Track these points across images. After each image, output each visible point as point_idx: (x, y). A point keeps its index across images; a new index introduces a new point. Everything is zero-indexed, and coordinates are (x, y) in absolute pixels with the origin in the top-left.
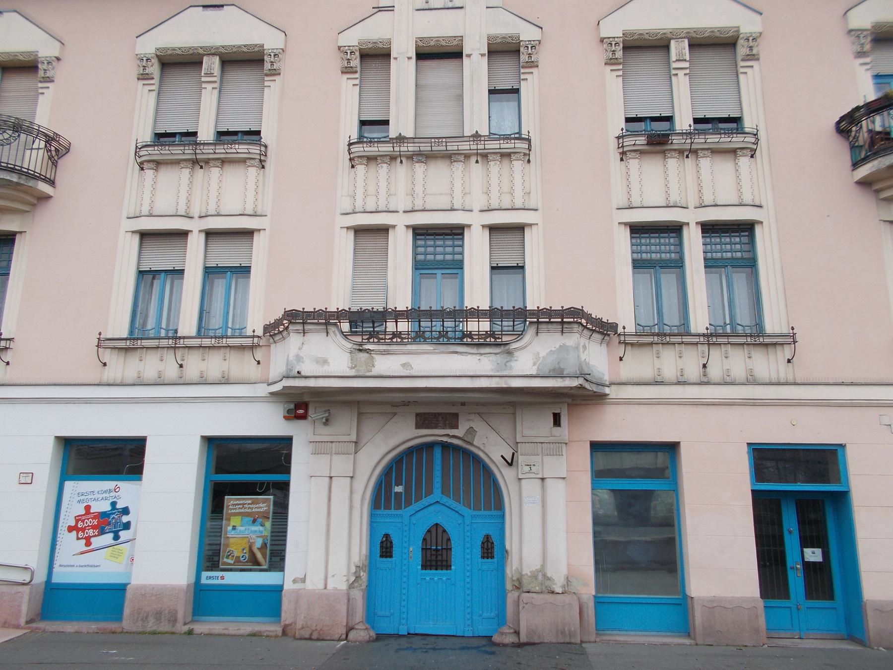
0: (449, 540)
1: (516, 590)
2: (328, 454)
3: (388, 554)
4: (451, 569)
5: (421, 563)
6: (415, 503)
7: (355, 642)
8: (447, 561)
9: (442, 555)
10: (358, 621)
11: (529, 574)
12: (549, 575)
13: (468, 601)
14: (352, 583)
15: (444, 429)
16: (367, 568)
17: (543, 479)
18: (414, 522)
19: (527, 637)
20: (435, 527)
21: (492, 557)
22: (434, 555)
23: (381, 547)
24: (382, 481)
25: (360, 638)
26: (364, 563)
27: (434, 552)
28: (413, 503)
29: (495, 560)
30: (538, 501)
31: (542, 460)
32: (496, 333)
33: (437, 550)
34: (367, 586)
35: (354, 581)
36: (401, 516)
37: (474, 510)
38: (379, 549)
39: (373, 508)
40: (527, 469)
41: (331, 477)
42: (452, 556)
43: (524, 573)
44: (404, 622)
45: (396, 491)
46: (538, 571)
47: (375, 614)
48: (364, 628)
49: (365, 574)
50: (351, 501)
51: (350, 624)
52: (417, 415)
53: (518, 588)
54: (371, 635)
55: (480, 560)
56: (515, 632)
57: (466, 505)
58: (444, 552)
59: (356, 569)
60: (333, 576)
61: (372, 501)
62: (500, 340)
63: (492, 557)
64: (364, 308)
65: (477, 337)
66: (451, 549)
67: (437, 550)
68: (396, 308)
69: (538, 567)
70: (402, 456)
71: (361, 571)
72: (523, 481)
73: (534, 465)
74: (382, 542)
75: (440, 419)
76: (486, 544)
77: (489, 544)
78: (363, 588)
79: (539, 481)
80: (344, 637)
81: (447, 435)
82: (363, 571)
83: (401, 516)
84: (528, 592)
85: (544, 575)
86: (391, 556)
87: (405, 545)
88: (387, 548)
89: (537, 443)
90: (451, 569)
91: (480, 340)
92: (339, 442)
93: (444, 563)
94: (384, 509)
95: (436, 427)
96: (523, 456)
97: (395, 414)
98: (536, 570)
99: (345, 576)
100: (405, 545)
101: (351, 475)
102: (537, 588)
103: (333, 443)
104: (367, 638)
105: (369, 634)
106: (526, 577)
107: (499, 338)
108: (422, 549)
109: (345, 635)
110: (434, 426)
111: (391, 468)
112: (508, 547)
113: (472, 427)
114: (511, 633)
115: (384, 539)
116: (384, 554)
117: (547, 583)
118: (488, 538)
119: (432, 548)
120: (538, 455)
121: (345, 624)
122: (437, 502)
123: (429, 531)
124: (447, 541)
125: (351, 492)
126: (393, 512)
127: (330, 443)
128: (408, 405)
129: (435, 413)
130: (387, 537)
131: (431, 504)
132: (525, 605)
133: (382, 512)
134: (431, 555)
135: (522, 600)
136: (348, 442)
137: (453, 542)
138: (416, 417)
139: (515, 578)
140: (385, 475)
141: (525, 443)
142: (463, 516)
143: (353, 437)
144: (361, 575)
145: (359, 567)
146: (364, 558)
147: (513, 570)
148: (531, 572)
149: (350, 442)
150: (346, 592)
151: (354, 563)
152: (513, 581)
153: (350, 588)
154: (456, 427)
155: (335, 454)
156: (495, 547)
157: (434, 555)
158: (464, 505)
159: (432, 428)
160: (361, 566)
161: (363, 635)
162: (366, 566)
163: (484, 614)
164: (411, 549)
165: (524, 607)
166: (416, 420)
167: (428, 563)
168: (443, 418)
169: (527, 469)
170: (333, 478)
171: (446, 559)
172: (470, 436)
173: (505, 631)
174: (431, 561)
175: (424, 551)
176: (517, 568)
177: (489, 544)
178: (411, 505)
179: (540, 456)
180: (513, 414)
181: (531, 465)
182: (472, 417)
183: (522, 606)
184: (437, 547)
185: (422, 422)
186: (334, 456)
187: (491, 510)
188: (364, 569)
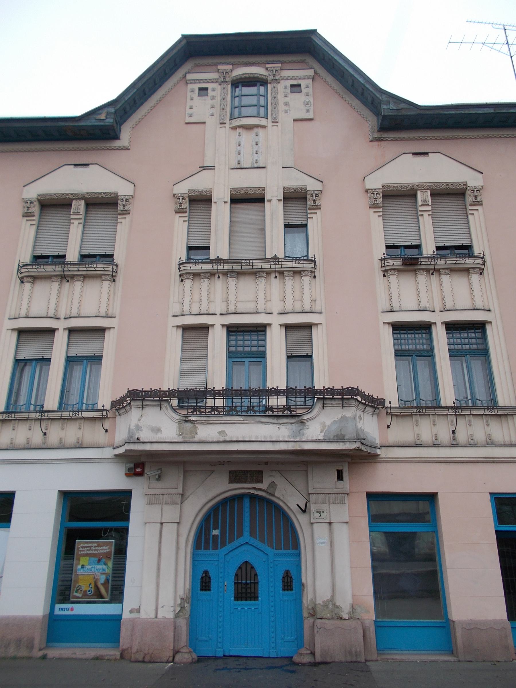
0: (256, 575)
5: (233, 595)
7: (180, 663)
8: (255, 593)
11: (322, 604)
12: (338, 604)
14: (178, 613)
15: (251, 483)
18: (228, 560)
23: (202, 582)
24: (202, 526)
25: (185, 660)
31: (329, 507)
32: (291, 407)
34: (190, 615)
36: (218, 555)
38: (199, 583)
39: (195, 548)
40: (317, 515)
41: (162, 524)
42: (259, 589)
43: (317, 602)
45: (213, 534)
46: (328, 601)
47: (197, 639)
48: (187, 651)
49: (188, 605)
51: (176, 649)
52: (231, 472)
58: (253, 585)
59: (181, 601)
60: (163, 607)
62: (295, 413)
63: (291, 590)
64: (189, 388)
65: (277, 410)
66: (258, 583)
67: (246, 584)
68: (333, 387)
69: (329, 597)
71: (185, 602)
72: (315, 525)
73: (323, 512)
74: (202, 578)
75: (249, 475)
76: (286, 578)
77: (289, 578)
79: (327, 525)
80: (171, 659)
82: (187, 603)
83: (218, 555)
84: (321, 619)
85: (334, 604)
91: (279, 413)
92: (169, 494)
93: (253, 595)
95: (245, 482)
97: (213, 472)
98: (328, 600)
104: (190, 660)
105: (192, 657)
106: (319, 606)
107: (294, 411)
112: (304, 581)
115: (204, 575)
116: (204, 588)
117: (337, 610)
118: (287, 573)
122: (247, 543)
123: (240, 568)
125: (178, 535)
126: (211, 552)
130: (206, 574)
131: (242, 545)
132: (318, 630)
133: (202, 552)
134: (242, 588)
139: (310, 607)
141: (316, 494)
142: (267, 554)
143: (180, 491)
144: (185, 606)
145: (184, 599)
146: (188, 592)
148: (323, 602)
149: (178, 494)
150: (173, 620)
151: (180, 596)
152: (309, 609)
153: (176, 617)
154: (261, 481)
155: (165, 504)
160: (185, 598)
161: (187, 657)
164: (226, 584)
165: (318, 631)
166: (230, 476)
167: (240, 595)
168: (250, 475)
174: (242, 593)
175: (236, 585)
176: (312, 599)
177: (289, 578)
178: (226, 545)
179: (328, 504)
184: (246, 581)
186: (166, 507)
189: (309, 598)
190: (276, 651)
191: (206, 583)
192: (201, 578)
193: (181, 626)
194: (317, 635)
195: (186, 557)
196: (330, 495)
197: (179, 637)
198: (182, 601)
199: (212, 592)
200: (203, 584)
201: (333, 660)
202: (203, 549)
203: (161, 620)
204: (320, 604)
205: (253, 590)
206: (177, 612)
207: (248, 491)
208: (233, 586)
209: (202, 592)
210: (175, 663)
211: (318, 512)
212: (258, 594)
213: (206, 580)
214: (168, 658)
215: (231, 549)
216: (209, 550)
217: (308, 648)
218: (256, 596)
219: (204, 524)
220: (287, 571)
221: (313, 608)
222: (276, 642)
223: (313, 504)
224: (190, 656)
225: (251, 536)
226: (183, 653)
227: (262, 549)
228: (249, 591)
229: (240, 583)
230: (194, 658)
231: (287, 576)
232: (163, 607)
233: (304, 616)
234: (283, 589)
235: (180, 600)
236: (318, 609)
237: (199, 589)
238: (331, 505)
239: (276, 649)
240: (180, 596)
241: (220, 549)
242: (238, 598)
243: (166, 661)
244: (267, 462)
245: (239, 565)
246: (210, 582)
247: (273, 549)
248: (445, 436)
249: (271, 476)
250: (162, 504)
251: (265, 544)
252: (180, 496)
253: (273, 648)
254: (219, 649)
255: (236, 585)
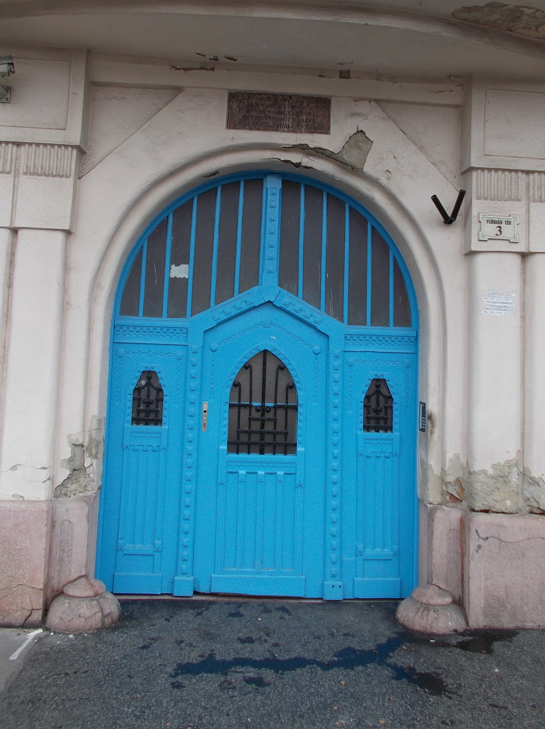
0: (291, 387)
1: (451, 504)
2: (9, 173)
3: (152, 416)
4: (294, 452)
5: (226, 437)
6: (216, 304)
7: (66, 632)
8: (286, 434)
9: (275, 421)
10: (74, 575)
11: (491, 472)
12: (536, 474)
13: (334, 523)
14: (63, 485)
15: (294, 132)
16: (102, 448)
17: (524, 256)
18: (214, 346)
19: (486, 615)
20: (260, 361)
21: (388, 428)
22: (256, 419)
23: (137, 400)
24: (141, 252)
25: (79, 623)
26: (94, 436)
27: (256, 415)
28: (212, 304)
29: (395, 434)
30: (513, 305)
31: (528, 211)
33: (263, 409)
34: (100, 488)
35: (68, 478)
36: (185, 331)
37: (349, 323)
38: (130, 404)
39: (118, 309)
40: (491, 230)
41: (15, 231)
42: (300, 424)
43: (477, 467)
44: (184, 566)
45: (172, 276)
46: (509, 464)
47: (118, 549)
48: (90, 593)
49: (95, 462)
50: (65, 289)
51: (55, 583)
52: (233, 96)
53: (455, 500)
54: (107, 611)
55: (362, 433)
56: (454, 602)
57: (331, 310)
58: (281, 414)
59: (73, 451)
60: (14, 468)
61: (116, 298)
63: (388, 428)
66: (295, 408)
67: (263, 409)
69: (512, 456)
70: (189, 198)
71: (87, 454)
72: (480, 260)
73: (508, 223)
74: (138, 390)
75: (287, 109)
76: (373, 399)
77: (382, 399)
78: (89, 493)
79: (517, 259)
80: (37, 616)
81: (303, 148)
82: (91, 455)
83: (185, 331)
84: (486, 511)
85: (524, 474)
86: (158, 422)
87: (192, 397)
88: (148, 403)
89: (516, 171)
90: (294, 452)
92: (38, 145)
93: (280, 439)
94: (146, 314)
95: (276, 127)
96: (482, 201)
97: (178, 90)
98: (508, 461)
99: (45, 468)
100: (192, 397)
101: (67, 227)
102: (508, 503)
103: (23, 148)
104: (96, 621)
105: (102, 610)
106: (482, 478)
108: (231, 406)
109: (41, 612)
110: (271, 124)
111: (165, 223)
112: (433, 407)
113: (362, 131)
114: (443, 606)
115: (143, 382)
116: (142, 415)
117: (530, 491)
118: (378, 386)
119: (254, 404)
120: (518, 200)
121: (41, 586)
122: (269, 302)
123: (247, 367)
124: (287, 390)
125: (66, 267)
126: (164, 321)
127: (15, 148)
128: (213, 69)
129: (275, 96)
130: (149, 379)
131: (255, 308)
132: (481, 542)
133: (140, 320)
134: (250, 420)
135: (477, 531)
136: (60, 146)
137: (300, 393)
138: (229, 101)
139: (450, 478)
140: (149, 238)
141: (490, 170)
142: (328, 336)
143: (75, 138)
144: (86, 465)
145: (82, 446)
146: (95, 426)
147: (447, 460)
148: (494, 466)
149: (66, 146)
150: (44, 507)
151: (69, 436)
152: (447, 484)
153: (56, 497)
154: (324, 129)
155: (25, 173)
156: (395, 406)
157: (256, 419)
158: (328, 312)
159: (266, 128)
160: (86, 444)
161: (88, 614)
162: (97, 446)
163: (368, 550)
164: (205, 407)
165: (479, 547)
166: (230, 108)
167: (244, 438)
168: (293, 107)
169: (491, 230)
170: (20, 232)
171: (283, 430)
172: (355, 152)
173: (432, 602)
174: (249, 433)
175: (235, 410)
176: (457, 456)
177: (382, 399)
178: (208, 307)
179: (523, 203)
180: (457, 107)
181: (501, 222)
182: (364, 107)
183: (477, 544)
184: (263, 401)
185: (243, 114)
186: (26, 182)
187: (365, 324)
188: (94, 451)
189: (449, 455)
190: (341, 583)
191: (148, 403)
192: (135, 389)
193: (70, 521)
194: (477, 556)
195: (90, 331)
196: (531, 176)
197: (63, 550)
198: (78, 451)
199: (164, 427)
200: (139, 406)
201: (520, 624)
202: (141, 313)
203: (8, 505)
204: (484, 472)
205: (280, 426)
206: (59, 481)
207: (284, 156)
208: (226, 415)
209: (136, 427)
210: (47, 629)
211: (493, 222)
212: (294, 436)
213: (148, 395)
214: (28, 613)
215: (224, 317)
216: (160, 316)
217: (442, 586)
218: (289, 441)
219: (145, 248)
220: (378, 380)
221: (458, 480)
222: (341, 561)
223: (479, 198)
224: (97, 609)
225: (280, 285)
226: (77, 601)
227: (311, 321)
228: (271, 429)
229: (245, 406)
230: (109, 614)
231: (378, 393)
232: (14, 468)
233: (431, 500)
234: (364, 427)
235: (69, 449)
236: (478, 486)
237: (130, 418)
238: (532, 205)
239: (341, 579)
240: (69, 436)
241: (192, 315)
242: (238, 444)
243: (20, 621)
244: (349, 72)
245: (246, 360)
246: (162, 400)
247: (342, 321)
248: (522, 183)
249: (354, 115)
250: (17, 175)
251: (319, 308)
252: (75, 152)
253: (334, 576)
254: (184, 578)
255: (235, 410)
